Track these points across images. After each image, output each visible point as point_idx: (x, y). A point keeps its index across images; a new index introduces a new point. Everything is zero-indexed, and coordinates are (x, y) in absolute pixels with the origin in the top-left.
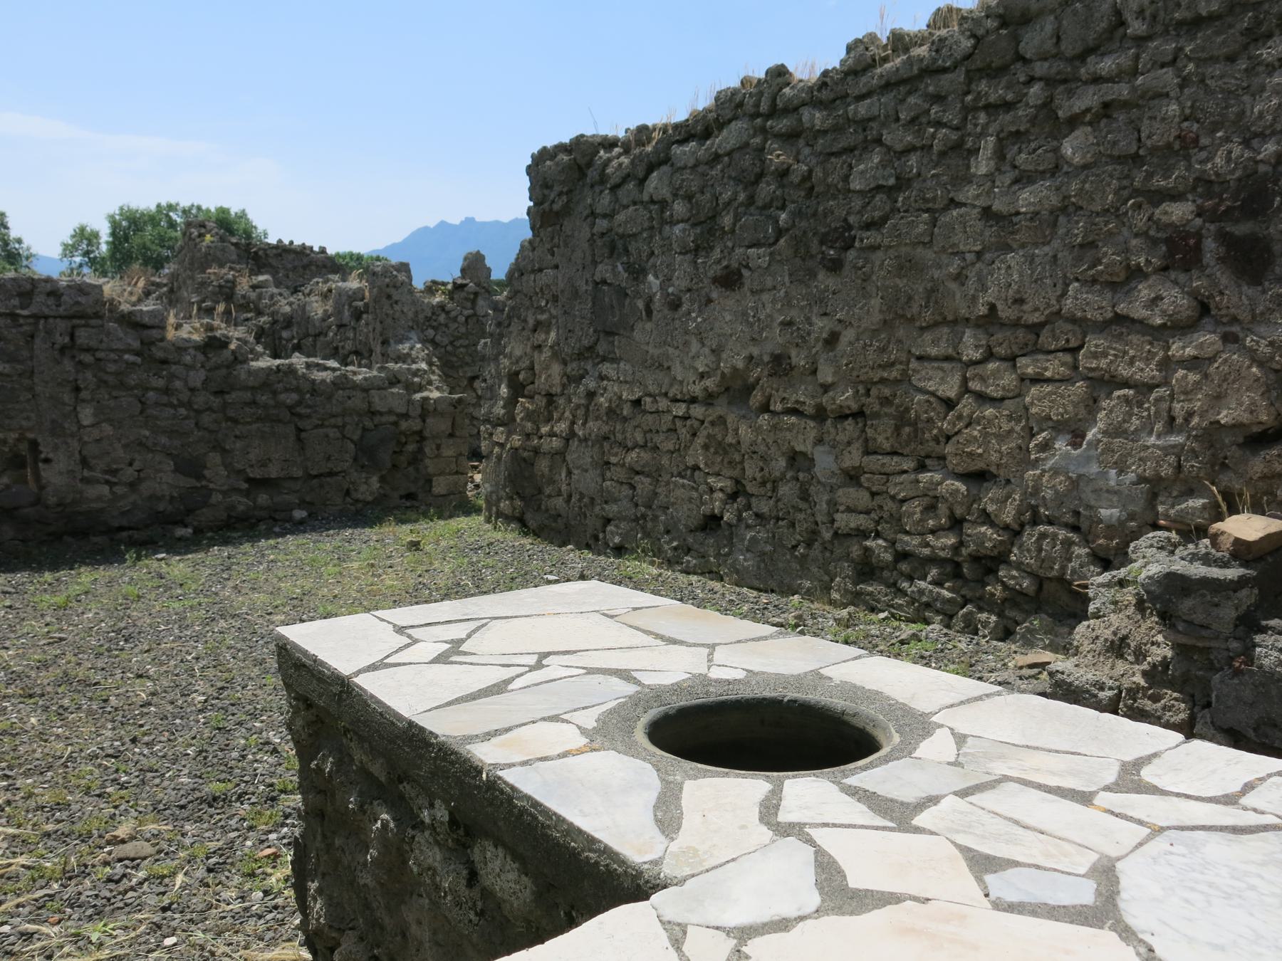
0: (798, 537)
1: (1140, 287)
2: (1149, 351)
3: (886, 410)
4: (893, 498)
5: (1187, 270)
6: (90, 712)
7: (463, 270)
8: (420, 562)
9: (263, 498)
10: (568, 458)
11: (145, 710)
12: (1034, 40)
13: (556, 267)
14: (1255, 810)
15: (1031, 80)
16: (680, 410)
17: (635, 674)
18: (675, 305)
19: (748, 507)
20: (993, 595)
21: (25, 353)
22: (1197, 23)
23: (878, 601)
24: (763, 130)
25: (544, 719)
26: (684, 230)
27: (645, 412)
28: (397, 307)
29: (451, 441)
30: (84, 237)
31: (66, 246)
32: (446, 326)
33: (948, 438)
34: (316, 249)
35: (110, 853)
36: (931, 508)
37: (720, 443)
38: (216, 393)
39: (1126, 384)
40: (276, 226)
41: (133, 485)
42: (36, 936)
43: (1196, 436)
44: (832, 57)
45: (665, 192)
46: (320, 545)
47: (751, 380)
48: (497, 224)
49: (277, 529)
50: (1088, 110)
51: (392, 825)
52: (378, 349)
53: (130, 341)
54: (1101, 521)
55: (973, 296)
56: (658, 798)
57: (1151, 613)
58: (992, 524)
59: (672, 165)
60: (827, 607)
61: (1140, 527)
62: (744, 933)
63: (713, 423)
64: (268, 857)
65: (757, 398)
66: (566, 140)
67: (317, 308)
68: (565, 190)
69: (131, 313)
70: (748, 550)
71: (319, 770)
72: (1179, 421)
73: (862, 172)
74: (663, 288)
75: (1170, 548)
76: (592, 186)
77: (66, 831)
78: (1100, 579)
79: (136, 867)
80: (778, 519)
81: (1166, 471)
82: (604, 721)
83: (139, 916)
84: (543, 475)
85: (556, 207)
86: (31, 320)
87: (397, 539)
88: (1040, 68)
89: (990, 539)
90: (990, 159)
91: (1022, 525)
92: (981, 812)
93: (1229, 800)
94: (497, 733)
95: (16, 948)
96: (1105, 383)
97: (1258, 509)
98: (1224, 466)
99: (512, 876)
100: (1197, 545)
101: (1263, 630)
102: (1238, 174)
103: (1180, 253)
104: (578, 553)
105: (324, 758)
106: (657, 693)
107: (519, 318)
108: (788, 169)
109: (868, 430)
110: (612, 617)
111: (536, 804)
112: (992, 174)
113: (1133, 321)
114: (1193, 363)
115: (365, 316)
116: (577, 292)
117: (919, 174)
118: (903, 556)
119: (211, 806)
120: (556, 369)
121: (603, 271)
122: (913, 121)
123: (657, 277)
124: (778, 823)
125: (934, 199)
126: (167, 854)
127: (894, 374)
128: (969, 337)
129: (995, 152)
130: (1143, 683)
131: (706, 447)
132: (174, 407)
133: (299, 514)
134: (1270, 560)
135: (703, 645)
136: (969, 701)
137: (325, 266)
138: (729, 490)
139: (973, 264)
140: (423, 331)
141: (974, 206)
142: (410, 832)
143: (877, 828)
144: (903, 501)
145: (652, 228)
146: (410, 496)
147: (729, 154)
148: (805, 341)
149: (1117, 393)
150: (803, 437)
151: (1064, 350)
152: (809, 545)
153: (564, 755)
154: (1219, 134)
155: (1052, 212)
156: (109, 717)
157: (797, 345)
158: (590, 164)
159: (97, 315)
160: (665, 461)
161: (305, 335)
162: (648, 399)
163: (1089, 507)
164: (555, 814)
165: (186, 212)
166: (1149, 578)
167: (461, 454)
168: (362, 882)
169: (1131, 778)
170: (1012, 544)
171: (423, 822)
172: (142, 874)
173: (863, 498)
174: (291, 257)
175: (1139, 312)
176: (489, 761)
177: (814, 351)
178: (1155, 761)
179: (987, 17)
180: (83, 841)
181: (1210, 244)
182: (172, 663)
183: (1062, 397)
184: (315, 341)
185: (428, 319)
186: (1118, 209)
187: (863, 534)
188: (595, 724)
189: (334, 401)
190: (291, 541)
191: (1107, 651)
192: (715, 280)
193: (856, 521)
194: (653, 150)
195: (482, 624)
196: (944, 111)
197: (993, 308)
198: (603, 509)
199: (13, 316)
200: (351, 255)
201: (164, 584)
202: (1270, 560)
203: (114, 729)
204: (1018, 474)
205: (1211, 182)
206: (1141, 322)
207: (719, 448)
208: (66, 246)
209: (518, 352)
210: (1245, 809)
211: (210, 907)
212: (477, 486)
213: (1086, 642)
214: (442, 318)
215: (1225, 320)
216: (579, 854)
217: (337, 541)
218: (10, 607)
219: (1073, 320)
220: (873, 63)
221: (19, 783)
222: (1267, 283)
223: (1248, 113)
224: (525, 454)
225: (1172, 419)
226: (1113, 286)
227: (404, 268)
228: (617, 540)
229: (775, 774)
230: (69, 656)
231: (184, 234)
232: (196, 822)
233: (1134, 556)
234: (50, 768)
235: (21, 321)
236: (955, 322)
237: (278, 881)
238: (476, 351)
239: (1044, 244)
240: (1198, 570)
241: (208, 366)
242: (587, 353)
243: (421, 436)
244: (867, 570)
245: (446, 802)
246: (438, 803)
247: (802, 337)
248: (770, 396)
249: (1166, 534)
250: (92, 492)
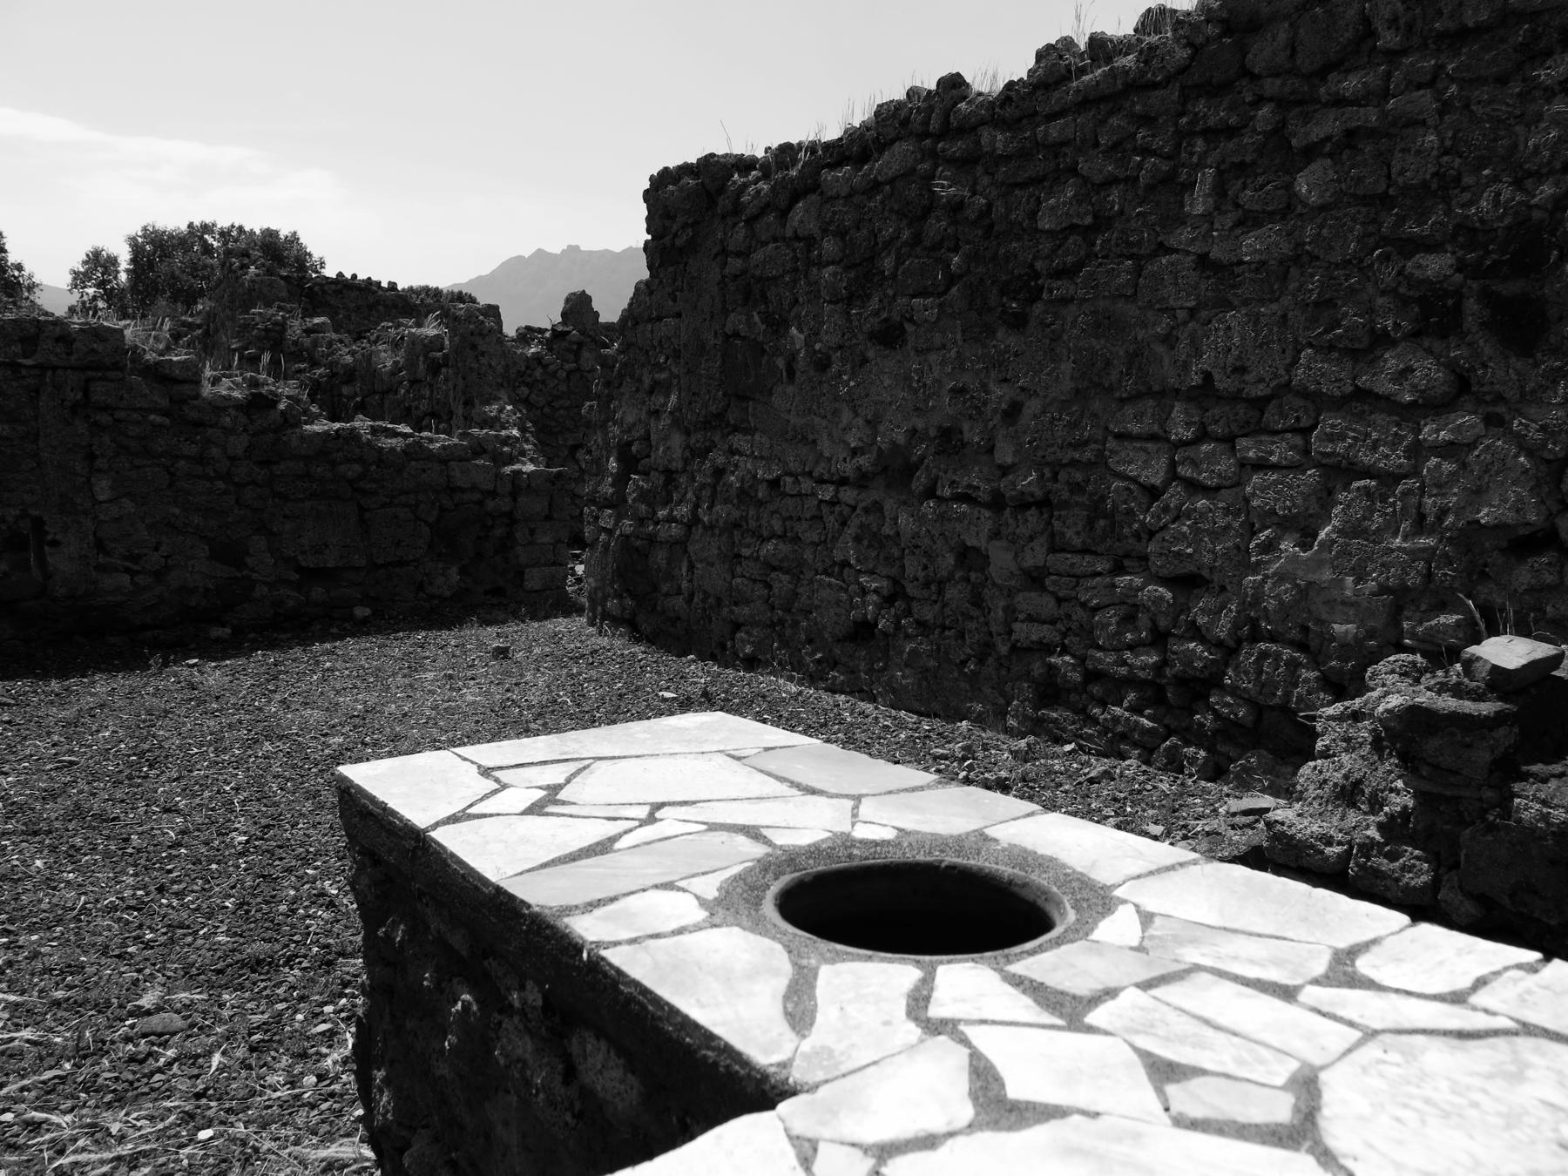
0: (968, 651)
1: (1387, 356)
2: (1396, 434)
4: (1084, 605)
5: (1444, 337)
6: (107, 854)
7: (563, 315)
8: (509, 674)
9: (318, 593)
10: (690, 549)
11: (174, 852)
12: (1264, 51)
13: (679, 315)
14: (1486, 1011)
15: (1259, 101)
16: (827, 493)
17: (765, 832)
18: (822, 364)
19: (908, 613)
20: (1202, 725)
22: (1461, 36)
23: (1064, 730)
24: (933, 154)
25: (656, 887)
26: (835, 274)
27: (785, 495)
28: (484, 360)
30: (99, 263)
31: (76, 274)
32: (543, 382)
33: (1152, 534)
34: (385, 284)
35: (132, 1027)
36: (1129, 619)
37: (875, 534)
39: (1367, 473)
40: (340, 252)
42: (45, 1126)
43: (1450, 538)
44: (1019, 66)
45: (812, 227)
46: (387, 651)
47: (915, 458)
48: (606, 254)
49: (334, 630)
50: (1328, 138)
51: (475, 1008)
52: (460, 410)
53: (156, 398)
54: (1333, 639)
55: (1185, 362)
56: (789, 986)
57: (1390, 755)
58: (1202, 640)
59: (822, 193)
60: (1002, 737)
61: (1380, 647)
62: (885, 1152)
63: (866, 510)
64: (323, 1033)
65: (920, 481)
66: (692, 159)
67: (386, 359)
68: (690, 221)
69: (158, 363)
70: (907, 666)
71: (389, 938)
72: (1431, 519)
73: (1052, 208)
74: (808, 344)
75: (1413, 674)
76: (724, 217)
77: (80, 999)
78: (1330, 711)
79: (165, 1045)
80: (944, 628)
81: (1413, 580)
83: (168, 1104)
85: (679, 242)
86: (37, 372)
87: (481, 645)
88: (1271, 86)
89: (1200, 658)
90: (1209, 195)
91: (1239, 642)
92: (1166, 1008)
93: (1457, 998)
94: (599, 903)
95: (21, 1140)
96: (1341, 471)
97: (1523, 630)
98: (1484, 576)
99: (617, 1074)
100: (1447, 672)
101: (1524, 777)
102: (1507, 221)
103: (1434, 316)
104: (700, 664)
105: (395, 926)
106: (791, 857)
107: (632, 377)
108: (962, 202)
109: (1056, 523)
110: (739, 759)
111: (646, 991)
112: (1210, 214)
113: (1378, 397)
114: (1448, 450)
115: (444, 370)
117: (1121, 212)
118: (1093, 676)
119: (254, 971)
120: (677, 440)
121: (736, 321)
122: (1115, 146)
124: (928, 1020)
125: (1139, 243)
126: (200, 1029)
127: (1088, 455)
128: (1178, 412)
129: (1214, 188)
130: (1378, 837)
131: (858, 539)
133: (361, 612)
134: (1534, 691)
135: (847, 796)
136: (1159, 871)
137: (395, 307)
138: (885, 592)
139: (1185, 323)
140: (514, 389)
141: (1188, 253)
142: (497, 1017)
143: (1044, 1027)
144: (1096, 609)
145: (796, 270)
146: (497, 591)
147: (892, 181)
148: (980, 413)
149: (1356, 484)
150: (977, 529)
151: (1293, 430)
152: (981, 661)
153: (680, 931)
154: (1486, 172)
155: (1281, 263)
156: (130, 860)
157: (971, 417)
158: (721, 190)
159: (117, 366)
160: (808, 555)
161: (375, 394)
162: (789, 479)
163: (1320, 622)
164: (667, 1004)
165: (225, 234)
166: (1387, 711)
167: (559, 541)
168: (438, 1073)
169: (1344, 970)
170: (1227, 665)
171: (511, 1006)
172: (171, 1053)
174: (355, 294)
175: (1385, 386)
176: (591, 938)
178: (1375, 949)
179: (1208, 21)
180: (100, 1012)
181: (1471, 305)
182: (207, 794)
183: (1290, 487)
185: (521, 374)
186: (1361, 261)
187: (1047, 648)
188: (716, 894)
189: (405, 475)
190: (351, 646)
191: (1337, 798)
192: (874, 337)
193: (1038, 633)
194: (798, 171)
195: (583, 766)
196: (1153, 136)
197: (1208, 377)
198: (732, 612)
199: (14, 366)
200: (426, 290)
201: (198, 698)
202: (1534, 691)
203: (136, 875)
204: (1235, 580)
205: (1475, 230)
206: (1387, 398)
207: (872, 539)
208: (76, 274)
209: (630, 419)
210: (1474, 1009)
211: (253, 1093)
212: (579, 580)
213: (1312, 787)
214: (538, 373)
215: (1488, 398)
216: (695, 1051)
217: (407, 646)
218: (9, 722)
219: (1305, 394)
220: (1068, 75)
221: (22, 940)
222: (1539, 355)
223: (1521, 148)
224: (638, 543)
225: (1422, 517)
226: (1354, 354)
227: (493, 311)
228: (748, 649)
229: (927, 958)
230: (82, 785)
231: (223, 265)
232: (236, 990)
233: (1371, 684)
234: (59, 922)
235: (24, 372)
236: (1162, 393)
237: (335, 1063)
238: (579, 413)
239: (1271, 301)
240: (1448, 703)
242: (715, 422)
243: (511, 519)
244: (1051, 691)
245: (540, 984)
246: (530, 984)
247: (977, 408)
248: (937, 478)
249: (1411, 658)
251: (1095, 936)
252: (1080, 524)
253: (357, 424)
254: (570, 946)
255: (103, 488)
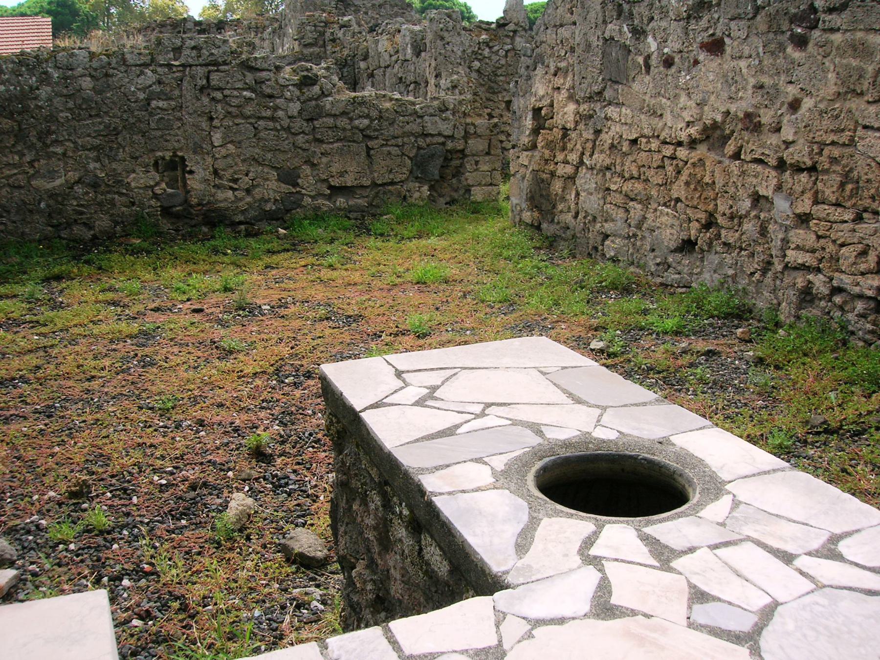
0: (756, 266)
3: (834, 168)
10: (577, 182)
13: (575, 24)
16: (668, 151)
21: (177, 93)
25: (472, 460)
28: (449, 48)
29: (487, 158)
32: (489, 58)
38: (308, 120)
41: (248, 191)
52: (432, 81)
65: (730, 148)
80: (741, 249)
82: (509, 465)
84: (556, 195)
86: (181, 68)
107: (543, 64)
116: (590, 46)
121: (612, 28)
123: (655, 38)
132: (278, 131)
144: (843, 245)
160: (654, 193)
162: (644, 140)
173: (810, 240)
177: (780, 112)
184: (384, 72)
188: (503, 468)
192: (704, 46)
193: (802, 258)
195: (453, 373)
209: (541, 92)
241: (302, 99)
248: (742, 146)
250: (221, 195)
251: (701, 514)
252: (836, 186)
253: (366, 93)
254: (421, 491)
255: (217, 138)
